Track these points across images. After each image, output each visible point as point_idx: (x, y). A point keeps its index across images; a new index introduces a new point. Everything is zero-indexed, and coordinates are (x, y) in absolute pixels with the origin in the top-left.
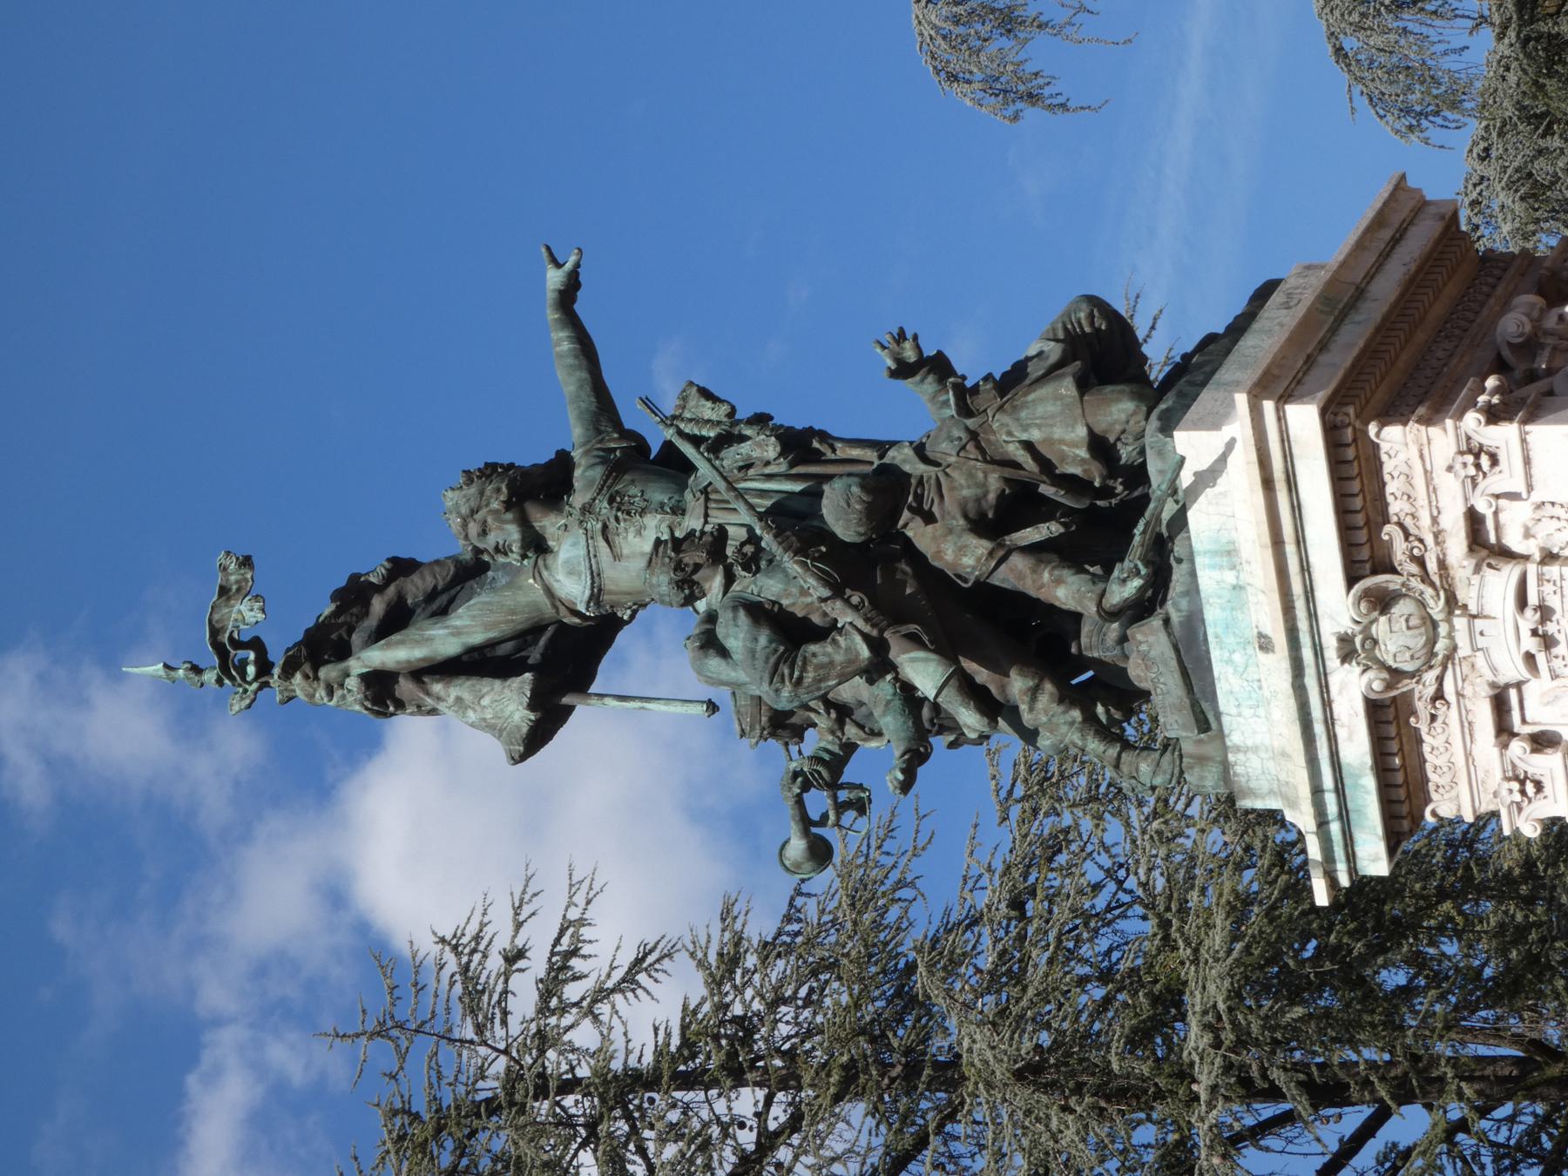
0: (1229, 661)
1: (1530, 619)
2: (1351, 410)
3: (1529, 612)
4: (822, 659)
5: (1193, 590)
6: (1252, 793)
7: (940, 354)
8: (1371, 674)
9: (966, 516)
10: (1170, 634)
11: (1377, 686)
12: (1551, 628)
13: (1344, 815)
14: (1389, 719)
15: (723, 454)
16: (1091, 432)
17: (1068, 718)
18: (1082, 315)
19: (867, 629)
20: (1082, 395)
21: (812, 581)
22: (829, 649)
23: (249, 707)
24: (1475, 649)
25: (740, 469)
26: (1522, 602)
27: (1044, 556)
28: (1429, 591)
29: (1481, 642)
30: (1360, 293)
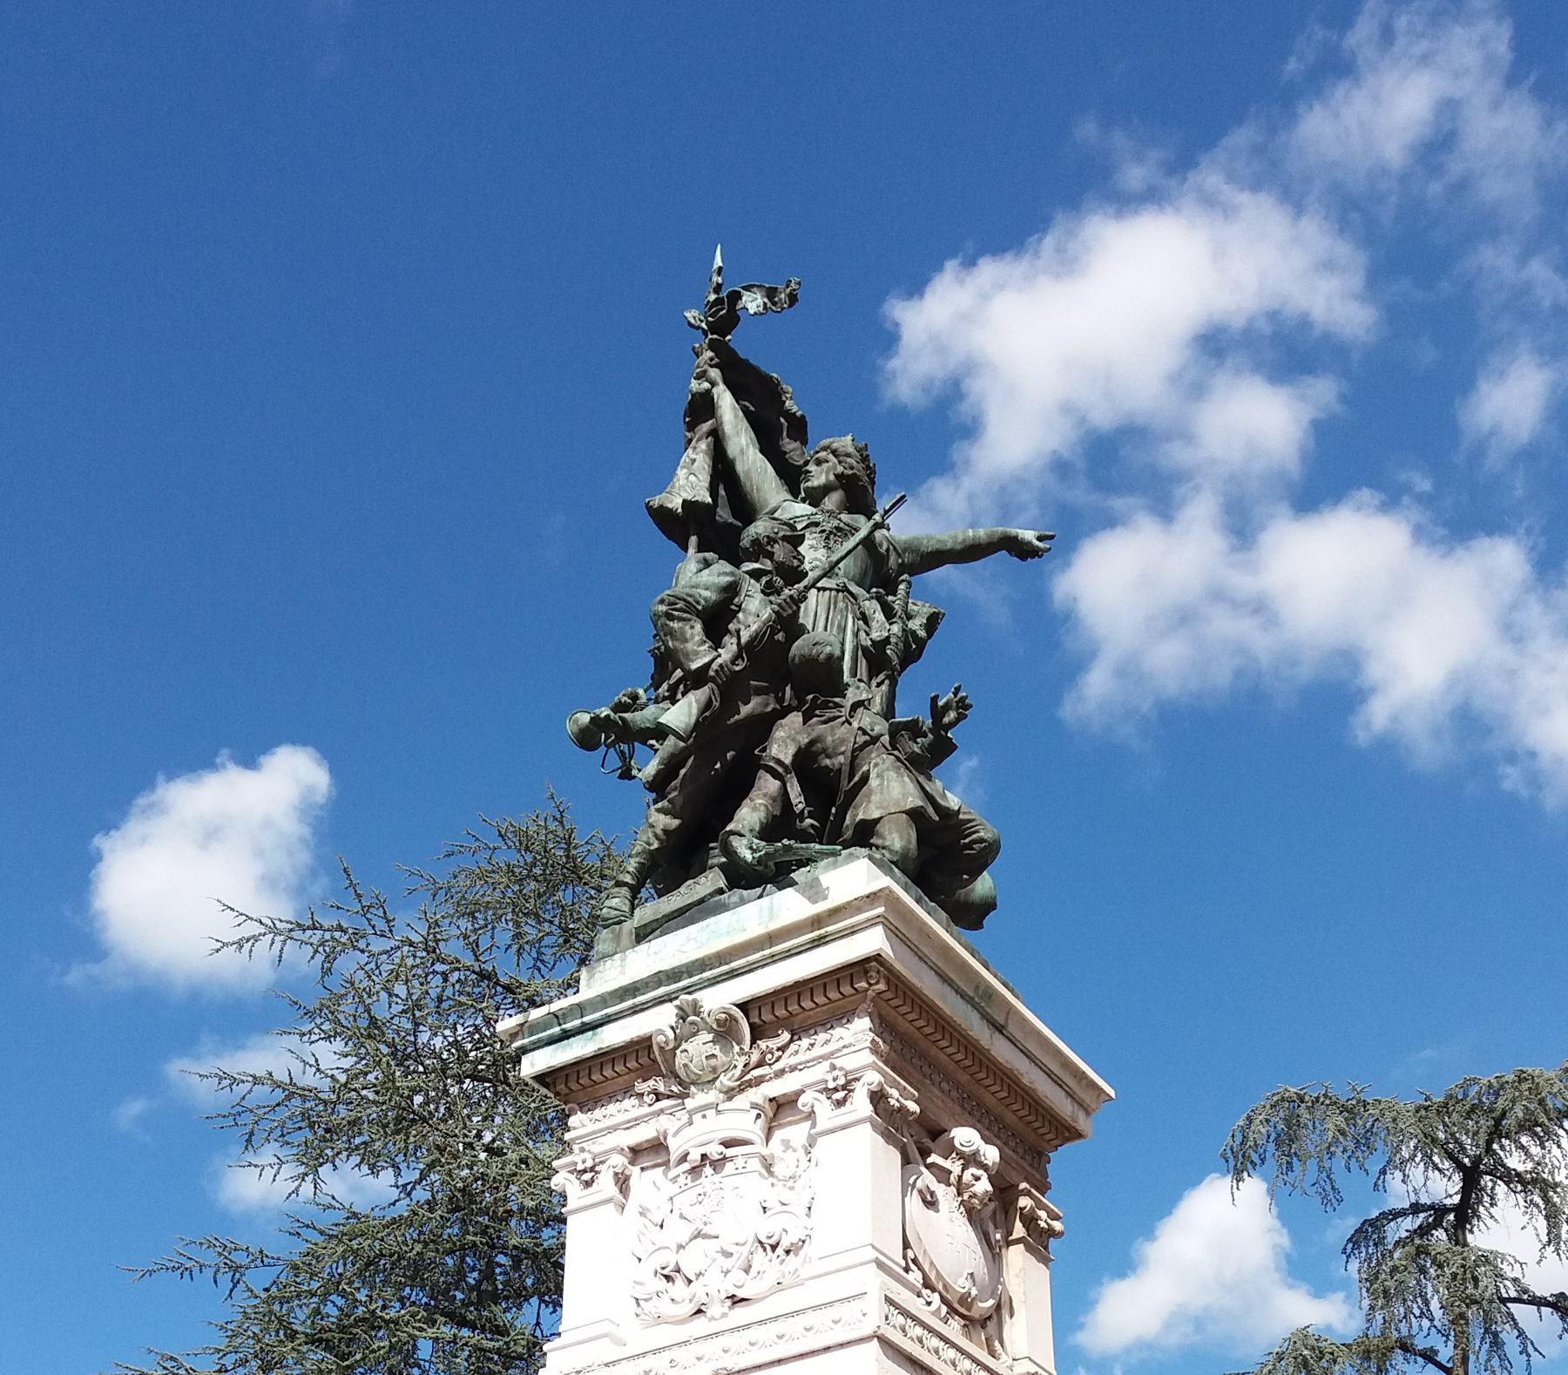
0: (689, 940)
1: (715, 1151)
2: (882, 986)
3: (722, 1148)
4: (689, 632)
5: (743, 902)
6: (591, 976)
7: (954, 747)
8: (671, 1035)
9: (812, 743)
10: (712, 895)
11: (661, 1038)
12: (708, 1170)
13: (566, 1035)
14: (641, 1059)
15: (874, 602)
16: (878, 820)
17: (653, 840)
18: (982, 834)
19: (715, 666)
20: (907, 812)
21: (754, 627)
22: (697, 638)
23: (690, 324)
24: (691, 1113)
25: (863, 614)
26: (728, 1144)
27: (779, 803)
28: (738, 1072)
29: (697, 1118)
30: (1000, 1029)
